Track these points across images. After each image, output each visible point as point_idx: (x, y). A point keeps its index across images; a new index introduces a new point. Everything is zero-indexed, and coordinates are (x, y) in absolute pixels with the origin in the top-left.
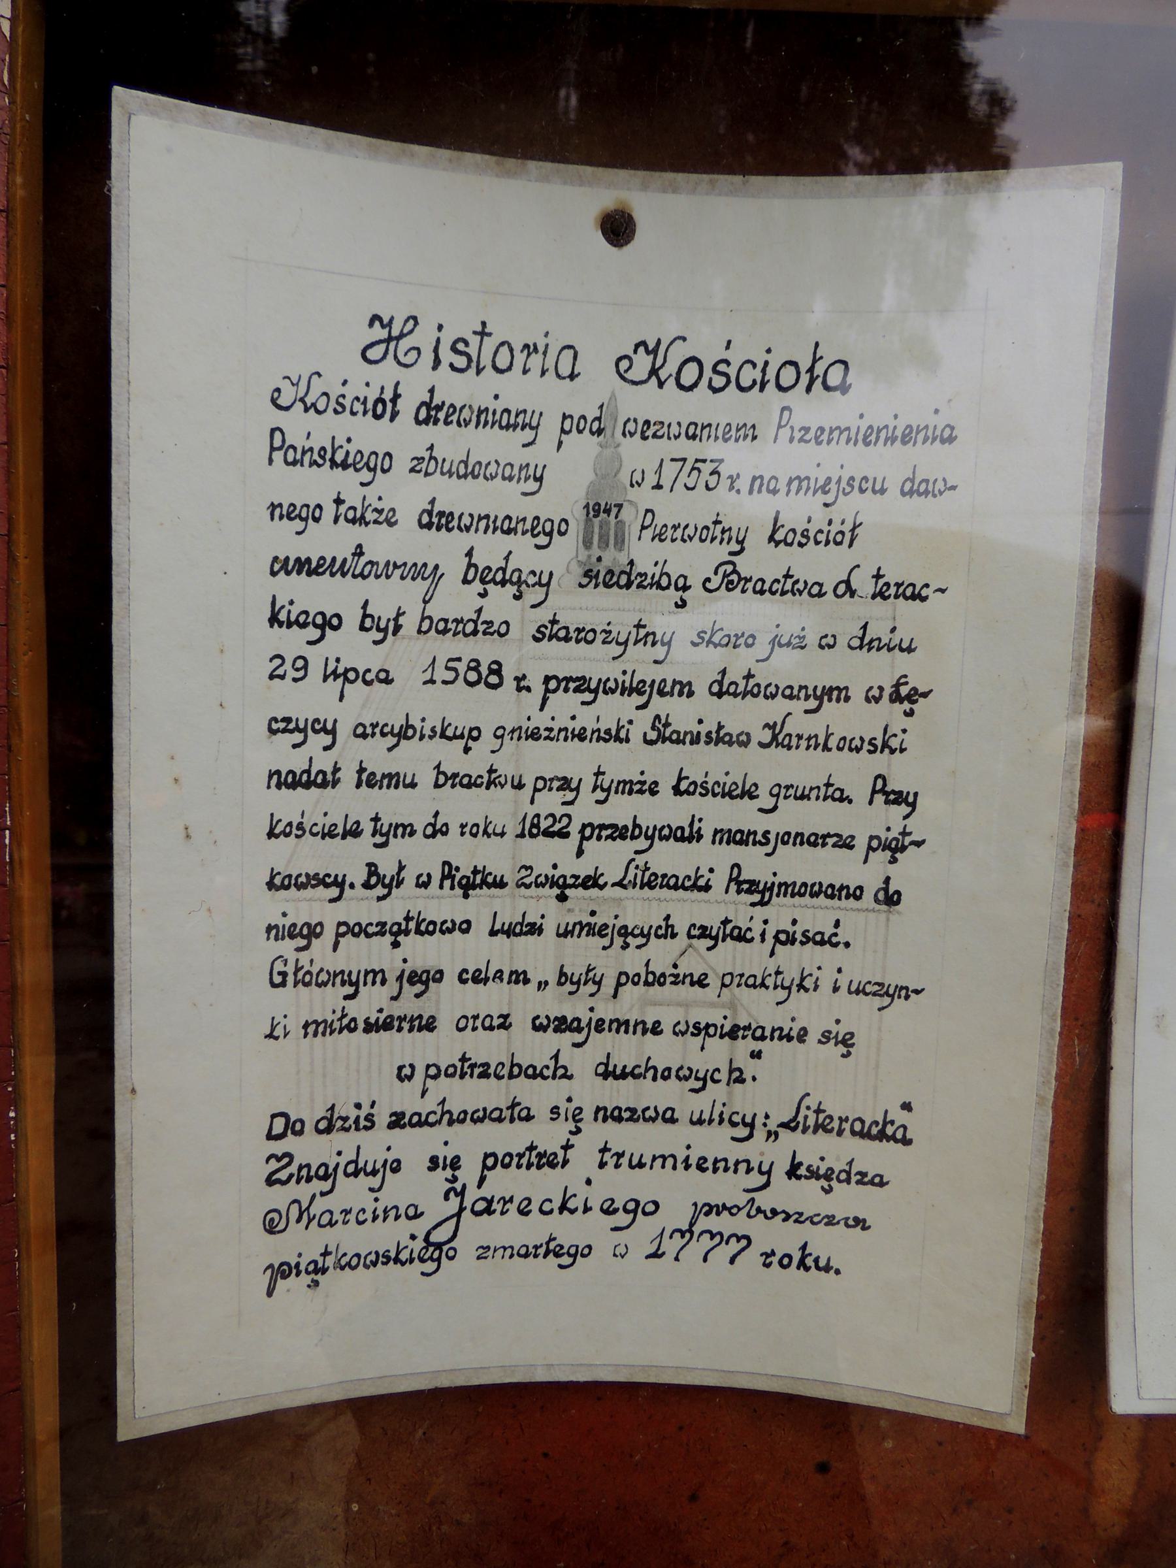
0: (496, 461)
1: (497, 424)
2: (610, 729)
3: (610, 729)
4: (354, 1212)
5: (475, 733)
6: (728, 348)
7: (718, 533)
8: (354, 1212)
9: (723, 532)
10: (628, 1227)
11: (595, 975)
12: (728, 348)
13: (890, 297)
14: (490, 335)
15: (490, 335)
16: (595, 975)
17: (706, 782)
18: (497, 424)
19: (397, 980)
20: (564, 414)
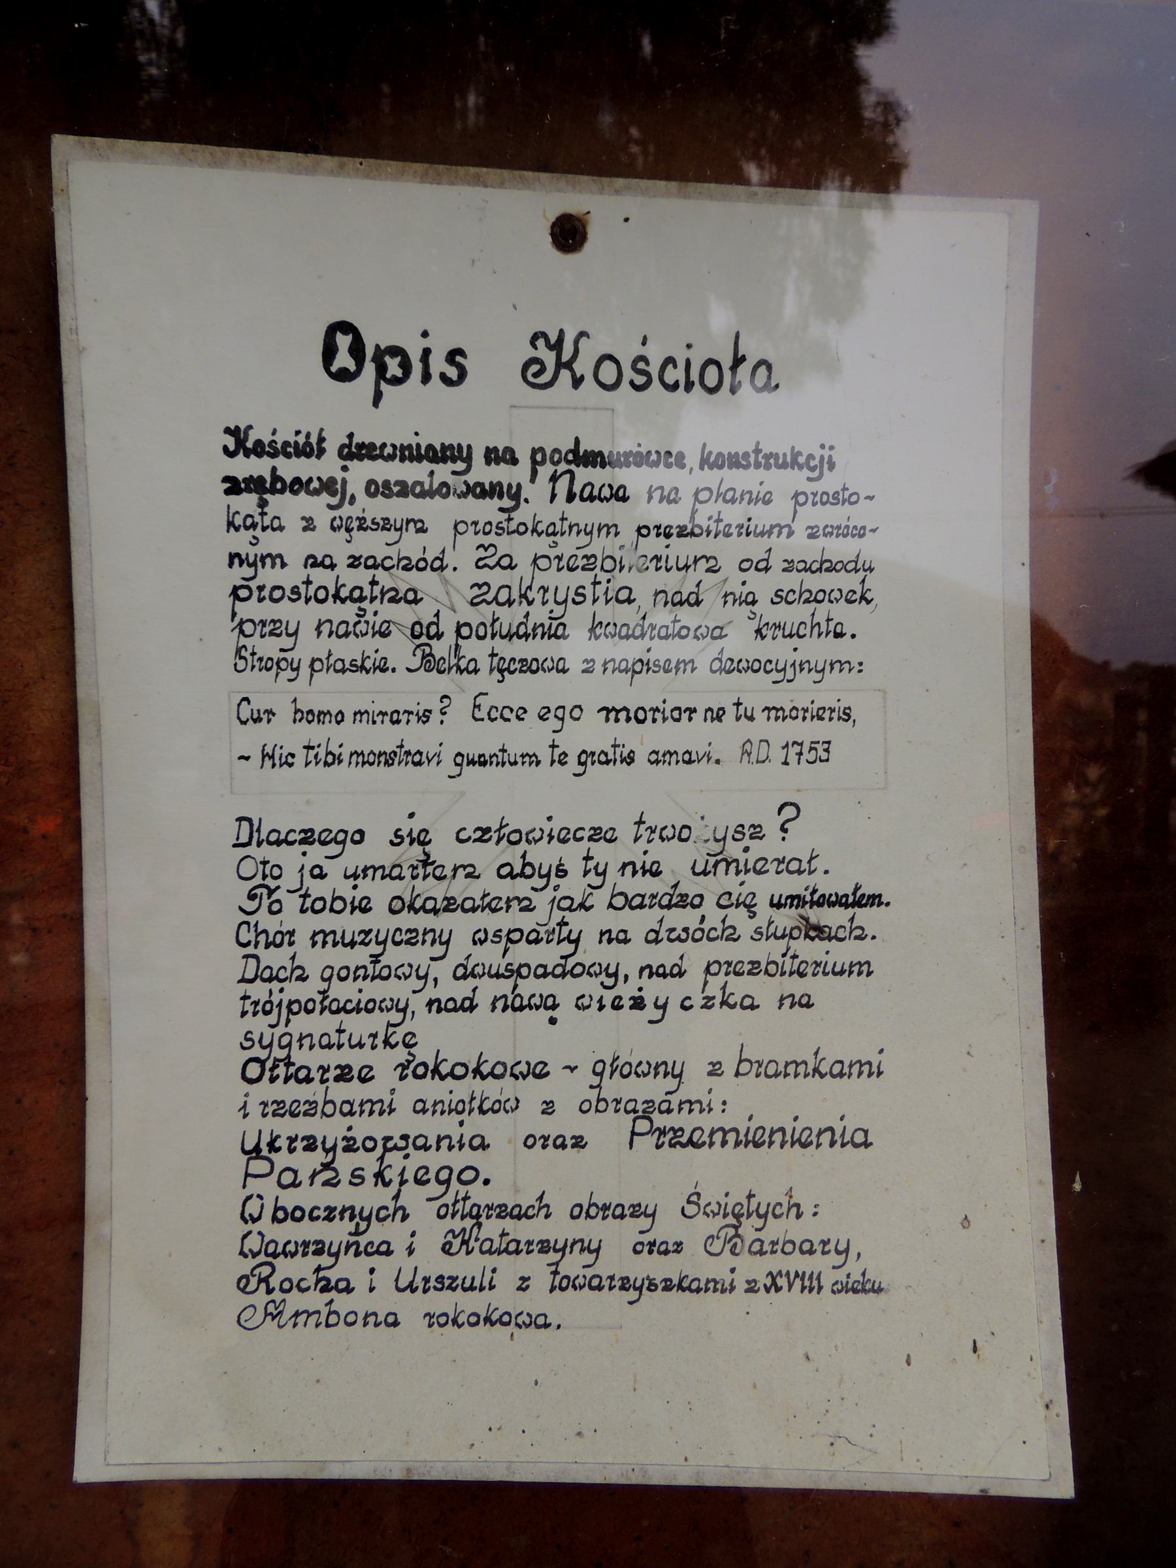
0: (590, 996)
1: (332, 668)
2: (688, 928)
3: (688, 928)
4: (261, 1004)
5: (530, 1142)
6: (644, 343)
7: (566, 528)
8: (261, 1004)
9: (571, 527)
10: (844, 1264)
11: (571, 931)
12: (644, 343)
13: (791, 306)
14: (558, 746)
15: (558, 746)
16: (571, 931)
17: (274, 441)
18: (332, 668)
19: (408, 1215)
20: (783, 763)
